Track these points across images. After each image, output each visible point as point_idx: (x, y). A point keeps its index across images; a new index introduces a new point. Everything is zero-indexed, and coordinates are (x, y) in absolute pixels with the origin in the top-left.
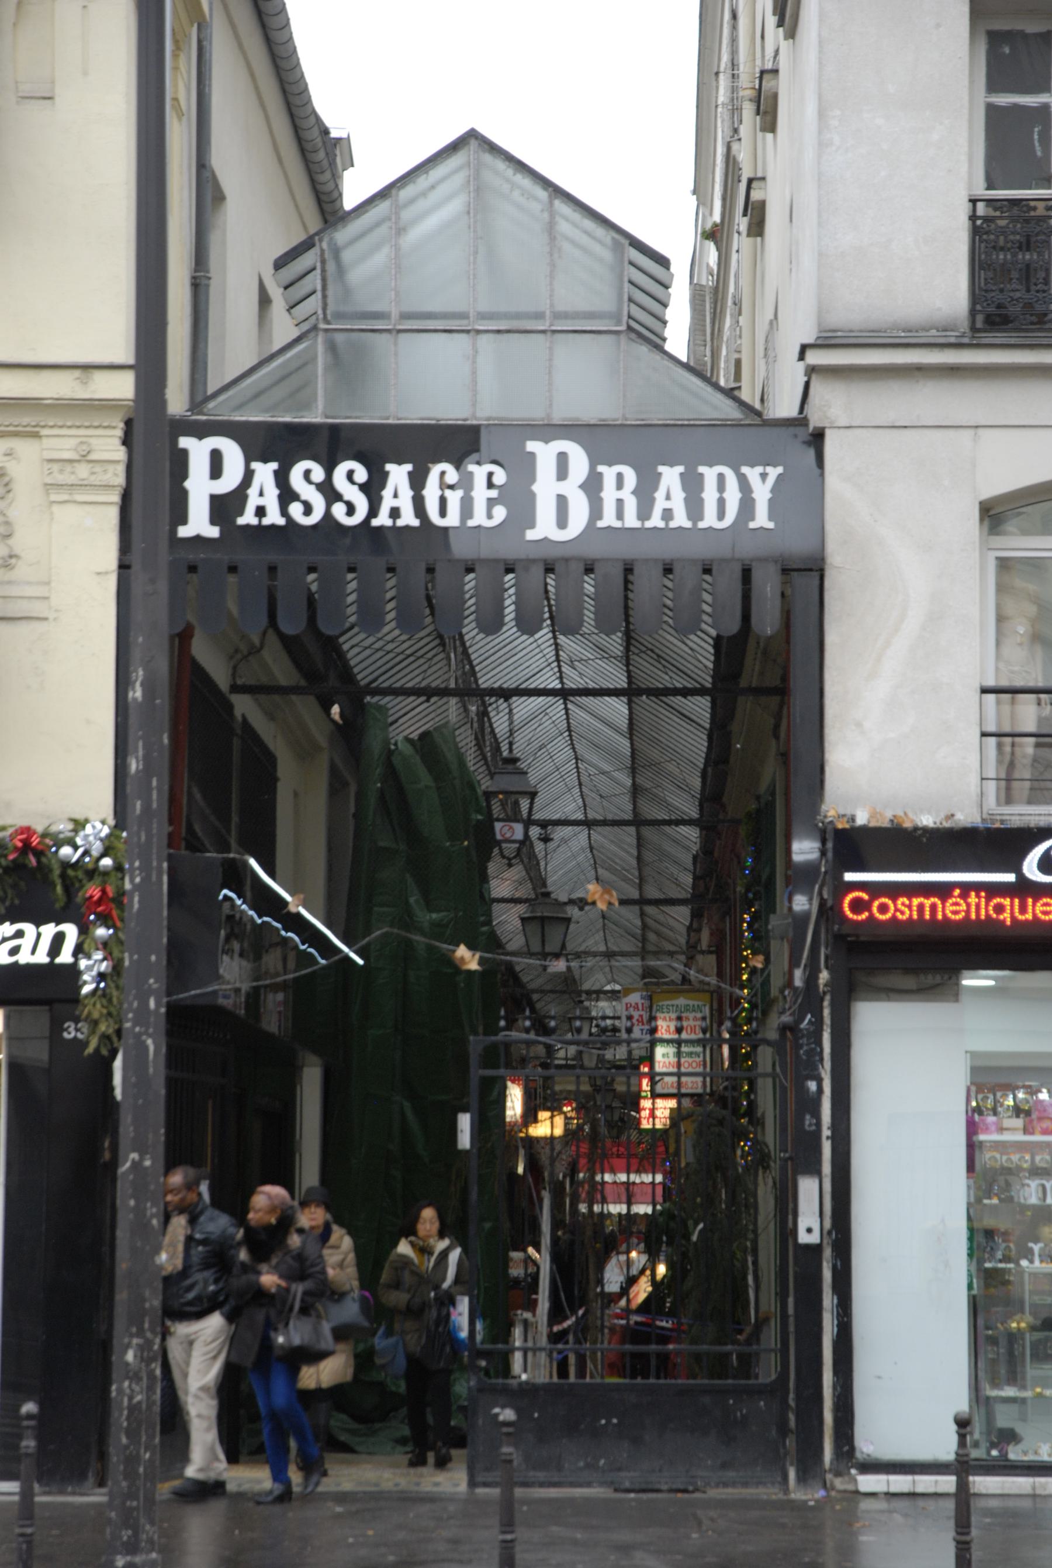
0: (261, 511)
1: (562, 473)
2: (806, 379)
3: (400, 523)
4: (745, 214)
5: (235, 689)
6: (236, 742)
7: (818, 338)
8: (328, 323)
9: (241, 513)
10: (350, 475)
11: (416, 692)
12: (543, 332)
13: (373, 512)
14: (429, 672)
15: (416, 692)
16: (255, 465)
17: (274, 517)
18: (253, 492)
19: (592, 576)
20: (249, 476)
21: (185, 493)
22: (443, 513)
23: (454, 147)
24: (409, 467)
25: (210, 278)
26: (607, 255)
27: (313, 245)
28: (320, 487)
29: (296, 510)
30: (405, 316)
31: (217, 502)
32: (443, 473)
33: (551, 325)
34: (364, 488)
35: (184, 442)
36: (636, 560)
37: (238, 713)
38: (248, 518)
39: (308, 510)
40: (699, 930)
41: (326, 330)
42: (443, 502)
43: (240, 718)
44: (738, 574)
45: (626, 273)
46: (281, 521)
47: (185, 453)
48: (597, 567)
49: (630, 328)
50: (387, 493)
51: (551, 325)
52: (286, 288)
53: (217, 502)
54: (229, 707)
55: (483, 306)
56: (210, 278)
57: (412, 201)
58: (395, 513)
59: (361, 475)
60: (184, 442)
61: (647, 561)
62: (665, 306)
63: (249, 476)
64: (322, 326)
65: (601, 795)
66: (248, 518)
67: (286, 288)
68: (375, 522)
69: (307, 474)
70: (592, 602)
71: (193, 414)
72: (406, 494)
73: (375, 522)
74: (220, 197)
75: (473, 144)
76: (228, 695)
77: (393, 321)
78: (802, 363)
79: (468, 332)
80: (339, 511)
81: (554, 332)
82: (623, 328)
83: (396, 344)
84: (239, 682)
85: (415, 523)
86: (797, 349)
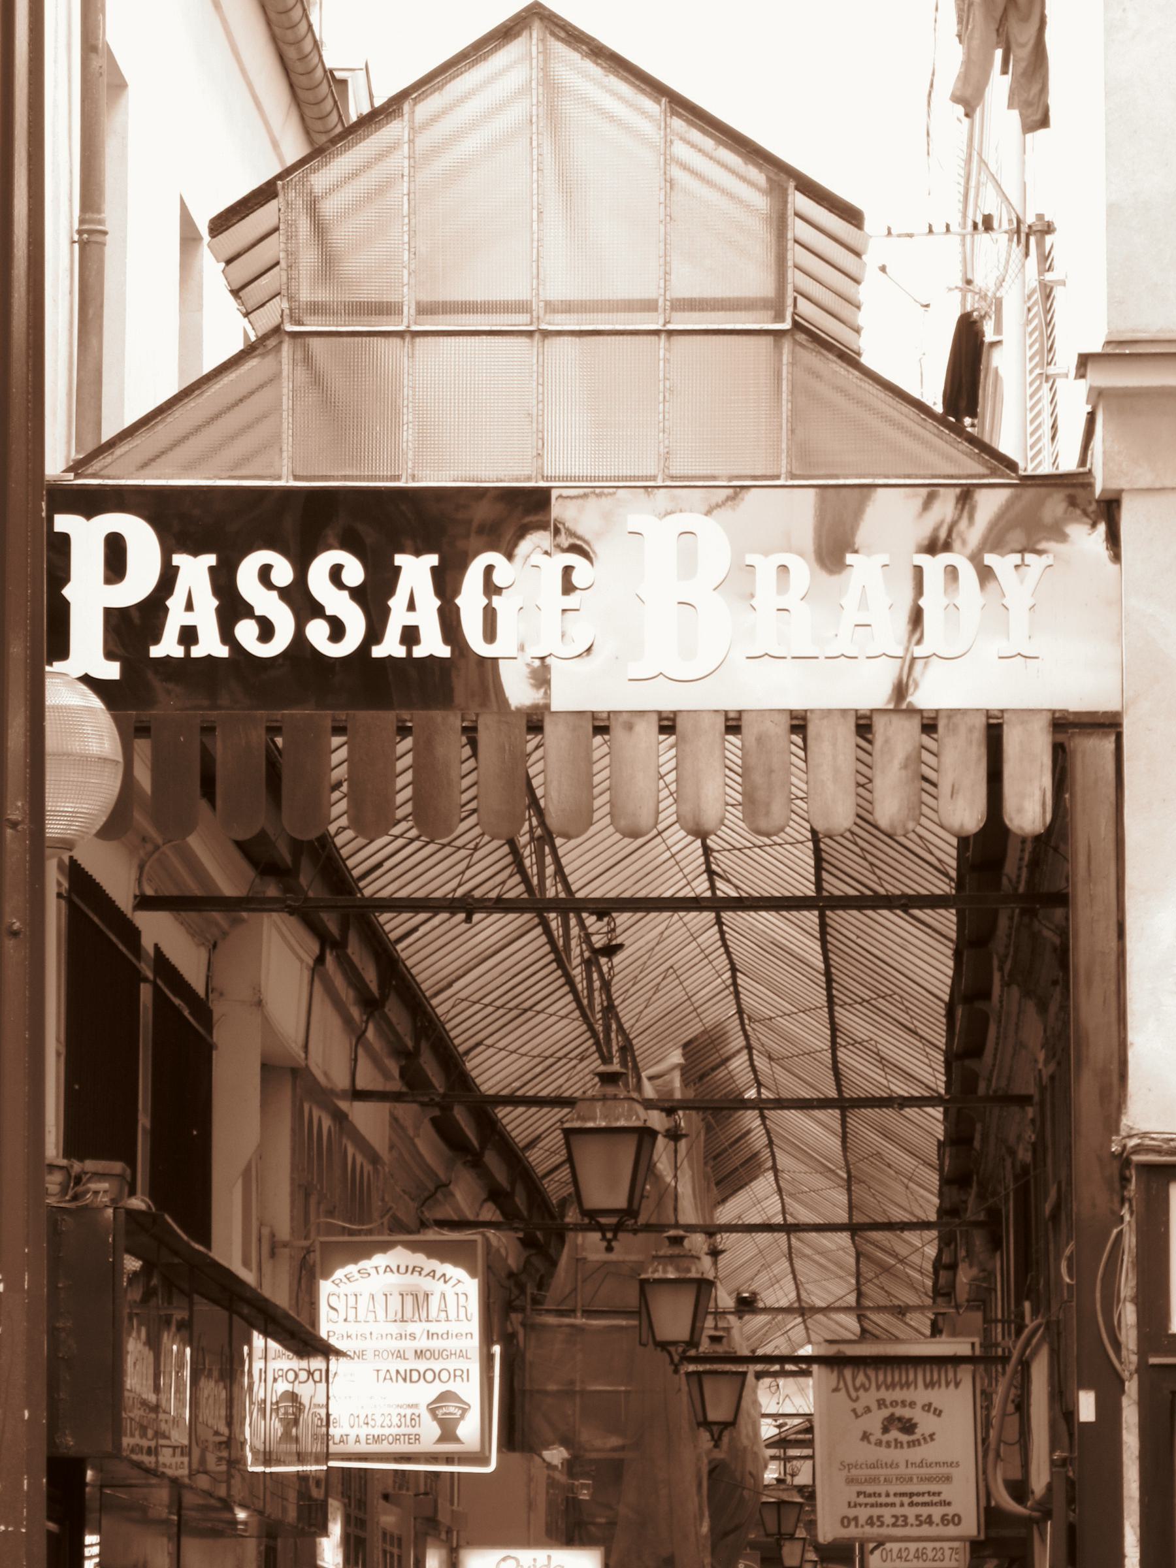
0: (188, 636)
1: (688, 565)
2: (1089, 408)
3: (419, 652)
4: (1005, 71)
5: (144, 903)
6: (146, 993)
7: (1108, 343)
8: (300, 323)
9: (157, 640)
10: (336, 573)
11: (451, 905)
12: (656, 333)
13: (374, 634)
14: (468, 874)
15: (451, 905)
16: (178, 559)
17: (210, 645)
18: (175, 603)
19: (740, 736)
20: (168, 578)
21: (65, 605)
22: (490, 634)
23: (506, 33)
24: (433, 559)
25: (105, 233)
26: (761, 202)
27: (275, 195)
28: (285, 594)
29: (246, 632)
30: (425, 309)
31: (116, 621)
32: (489, 569)
33: (666, 323)
34: (357, 594)
35: (64, 523)
36: (812, 711)
37: (147, 943)
38: (168, 647)
39: (267, 631)
40: (953, 1267)
41: (295, 335)
42: (490, 616)
43: (151, 951)
44: (979, 735)
45: (790, 255)
46: (223, 652)
47: (65, 539)
48: (745, 723)
49: (796, 324)
50: (397, 603)
51: (666, 323)
52: (229, 262)
53: (116, 621)
54: (132, 934)
55: (557, 291)
56: (105, 233)
57: (434, 119)
58: (410, 636)
59: (355, 574)
60: (64, 523)
61: (828, 713)
62: (857, 282)
63: (168, 578)
64: (289, 328)
65: (770, 1058)
66: (168, 647)
67: (229, 262)
68: (378, 652)
69: (265, 573)
70: (739, 779)
71: (77, 476)
72: (429, 603)
73: (378, 652)
74: (119, 86)
75: (537, 29)
76: (129, 915)
77: (405, 321)
78: (1083, 381)
79: (530, 334)
80: (317, 632)
81: (671, 333)
82: (787, 325)
83: (412, 356)
84: (149, 892)
85: (444, 652)
86: (1074, 361)
